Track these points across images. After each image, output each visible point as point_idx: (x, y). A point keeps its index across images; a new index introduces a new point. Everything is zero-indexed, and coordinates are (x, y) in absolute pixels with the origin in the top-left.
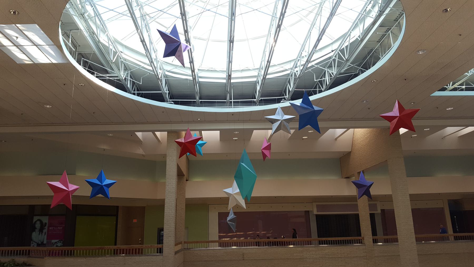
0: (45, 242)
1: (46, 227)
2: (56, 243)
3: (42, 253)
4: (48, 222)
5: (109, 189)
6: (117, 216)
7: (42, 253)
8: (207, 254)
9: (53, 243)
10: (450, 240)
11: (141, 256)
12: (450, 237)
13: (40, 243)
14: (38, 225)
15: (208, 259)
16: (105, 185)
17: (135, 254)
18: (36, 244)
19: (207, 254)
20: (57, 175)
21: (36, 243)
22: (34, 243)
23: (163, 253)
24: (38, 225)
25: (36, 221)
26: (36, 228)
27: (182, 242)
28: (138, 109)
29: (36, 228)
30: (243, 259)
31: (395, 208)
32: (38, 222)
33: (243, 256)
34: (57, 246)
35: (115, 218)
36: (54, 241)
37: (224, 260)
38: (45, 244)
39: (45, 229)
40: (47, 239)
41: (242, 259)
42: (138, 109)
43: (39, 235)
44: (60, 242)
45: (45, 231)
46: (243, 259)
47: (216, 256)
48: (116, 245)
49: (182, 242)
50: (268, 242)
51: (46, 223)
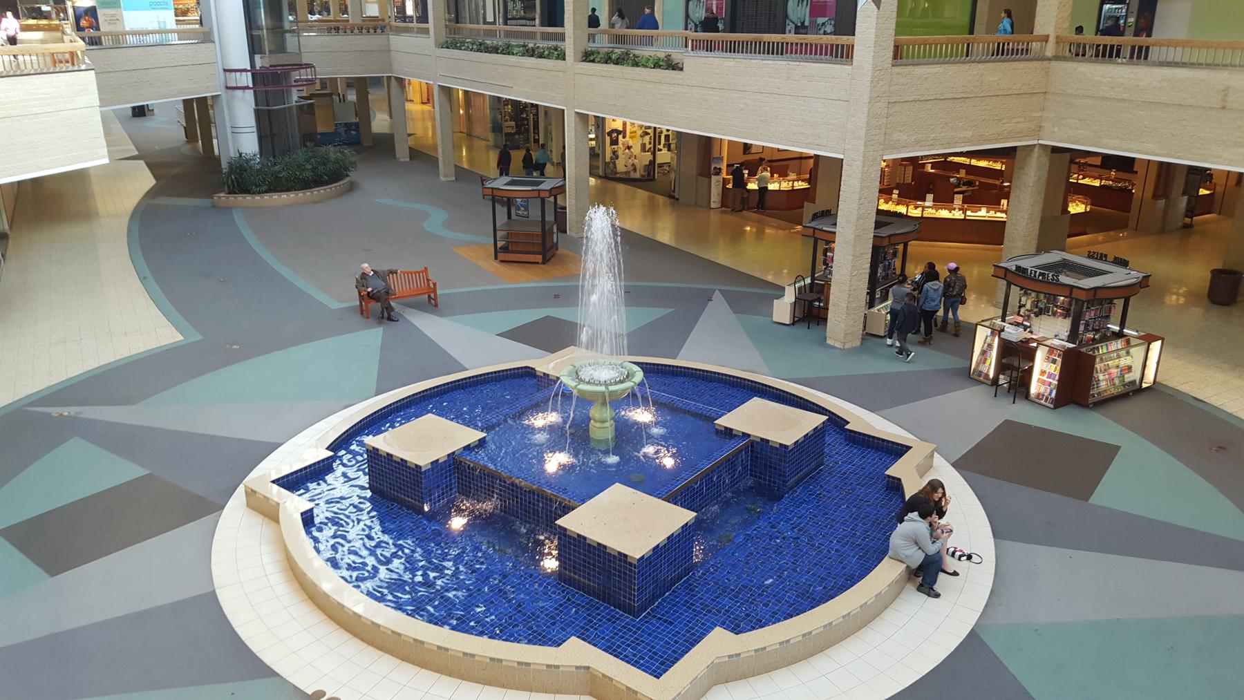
0: (807, 24)
3: (743, 47)
7: (743, 47)
12: (103, 37)
15: (1112, 93)
18: (793, 26)
20: (555, 216)
21: (793, 23)
22: (790, 23)
23: (852, 58)
27: (1048, 36)
28: (312, 643)
30: (1224, 108)
33: (1226, 95)
34: (825, 33)
37: (1157, 103)
38: (807, 27)
40: (810, 16)
41: (1220, 106)
42: (312, 643)
43: (798, 5)
44: (831, 24)
46: (1224, 108)
47: (1138, 86)
48: (973, 34)
49: (1048, 36)
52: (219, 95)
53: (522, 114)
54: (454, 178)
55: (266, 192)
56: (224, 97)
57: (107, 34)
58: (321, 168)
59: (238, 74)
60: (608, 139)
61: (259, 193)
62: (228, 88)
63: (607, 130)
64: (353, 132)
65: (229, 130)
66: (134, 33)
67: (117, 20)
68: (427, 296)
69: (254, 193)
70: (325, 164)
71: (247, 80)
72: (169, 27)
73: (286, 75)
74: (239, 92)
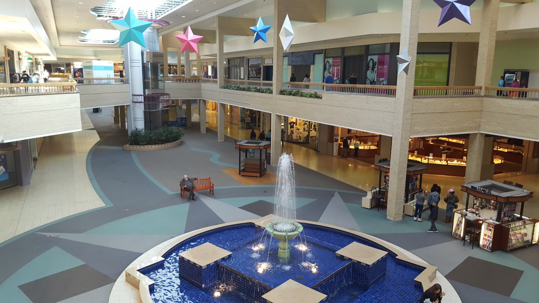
0: (375, 80)
1: (376, 66)
2: (383, 81)
4: (185, 63)
5: (143, 33)
6: (450, 53)
8: (510, 105)
9: (380, 81)
10: (84, 83)
11: (392, 97)
12: (84, 80)
13: (372, 81)
14: (371, 65)
15: (511, 112)
16: (135, 28)
17: (390, 94)
18: (370, 81)
19: (510, 105)
21: (370, 80)
22: (368, 80)
24: (371, 65)
25: (369, 61)
26: (370, 67)
29: (370, 67)
31: (480, 42)
32: (371, 61)
34: (383, 84)
35: (448, 56)
36: (381, 79)
39: (376, 67)
40: (377, 77)
43: (372, 73)
45: (376, 69)
47: (523, 108)
50: (500, 95)
51: (376, 62)
52: (130, 105)
53: (254, 115)
54: (224, 140)
55: (146, 144)
56: (131, 106)
57: (86, 79)
58: (170, 135)
59: (138, 97)
60: (289, 126)
61: (143, 145)
62: (133, 102)
63: (289, 122)
64: (184, 121)
65: (132, 119)
66: (97, 79)
67: (90, 74)
68: (209, 190)
69: (141, 145)
70: (171, 134)
71: (141, 99)
72: (111, 77)
73: (158, 98)
74: (138, 104)
